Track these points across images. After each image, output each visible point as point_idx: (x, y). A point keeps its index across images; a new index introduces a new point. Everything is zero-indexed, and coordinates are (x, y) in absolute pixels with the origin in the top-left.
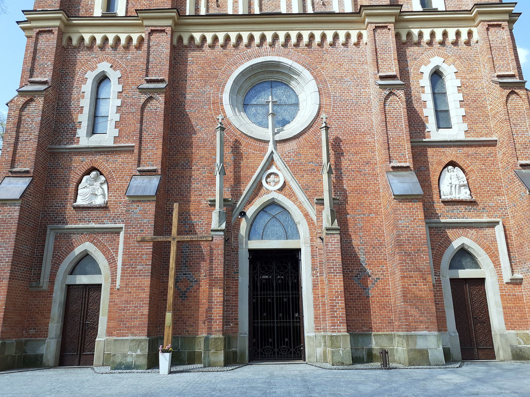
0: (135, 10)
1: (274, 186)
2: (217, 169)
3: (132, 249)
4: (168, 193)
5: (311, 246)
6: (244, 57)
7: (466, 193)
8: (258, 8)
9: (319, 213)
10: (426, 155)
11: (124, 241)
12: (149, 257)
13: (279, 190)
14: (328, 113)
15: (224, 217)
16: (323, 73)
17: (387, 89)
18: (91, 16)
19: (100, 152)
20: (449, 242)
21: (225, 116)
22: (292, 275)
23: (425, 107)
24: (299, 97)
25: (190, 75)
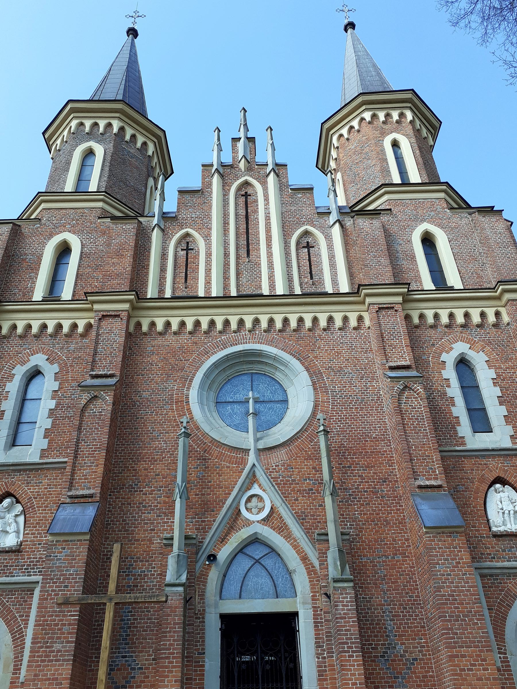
0: (84, 293)
1: (257, 514)
2: (177, 490)
3: (49, 616)
4: (107, 528)
5: (314, 607)
6: (217, 346)
9: (323, 555)
11: (39, 604)
12: (73, 629)
13: (264, 520)
14: (327, 412)
15: (184, 562)
16: (316, 363)
17: (400, 383)
18: (29, 300)
19: (19, 471)
22: (287, 655)
23: (454, 405)
24: (288, 392)
25: (149, 368)
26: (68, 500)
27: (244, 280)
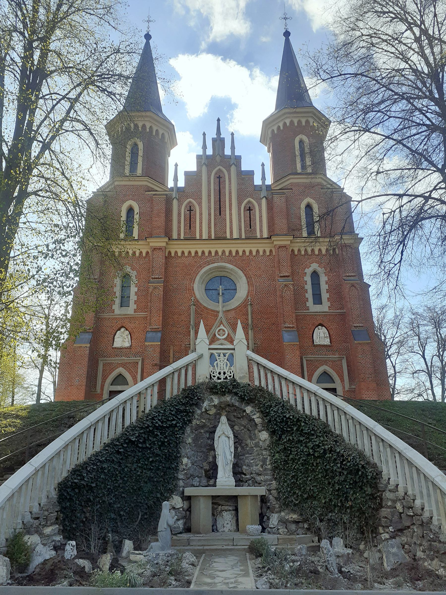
13: (225, 338)
24: (237, 285)
26: (150, 330)
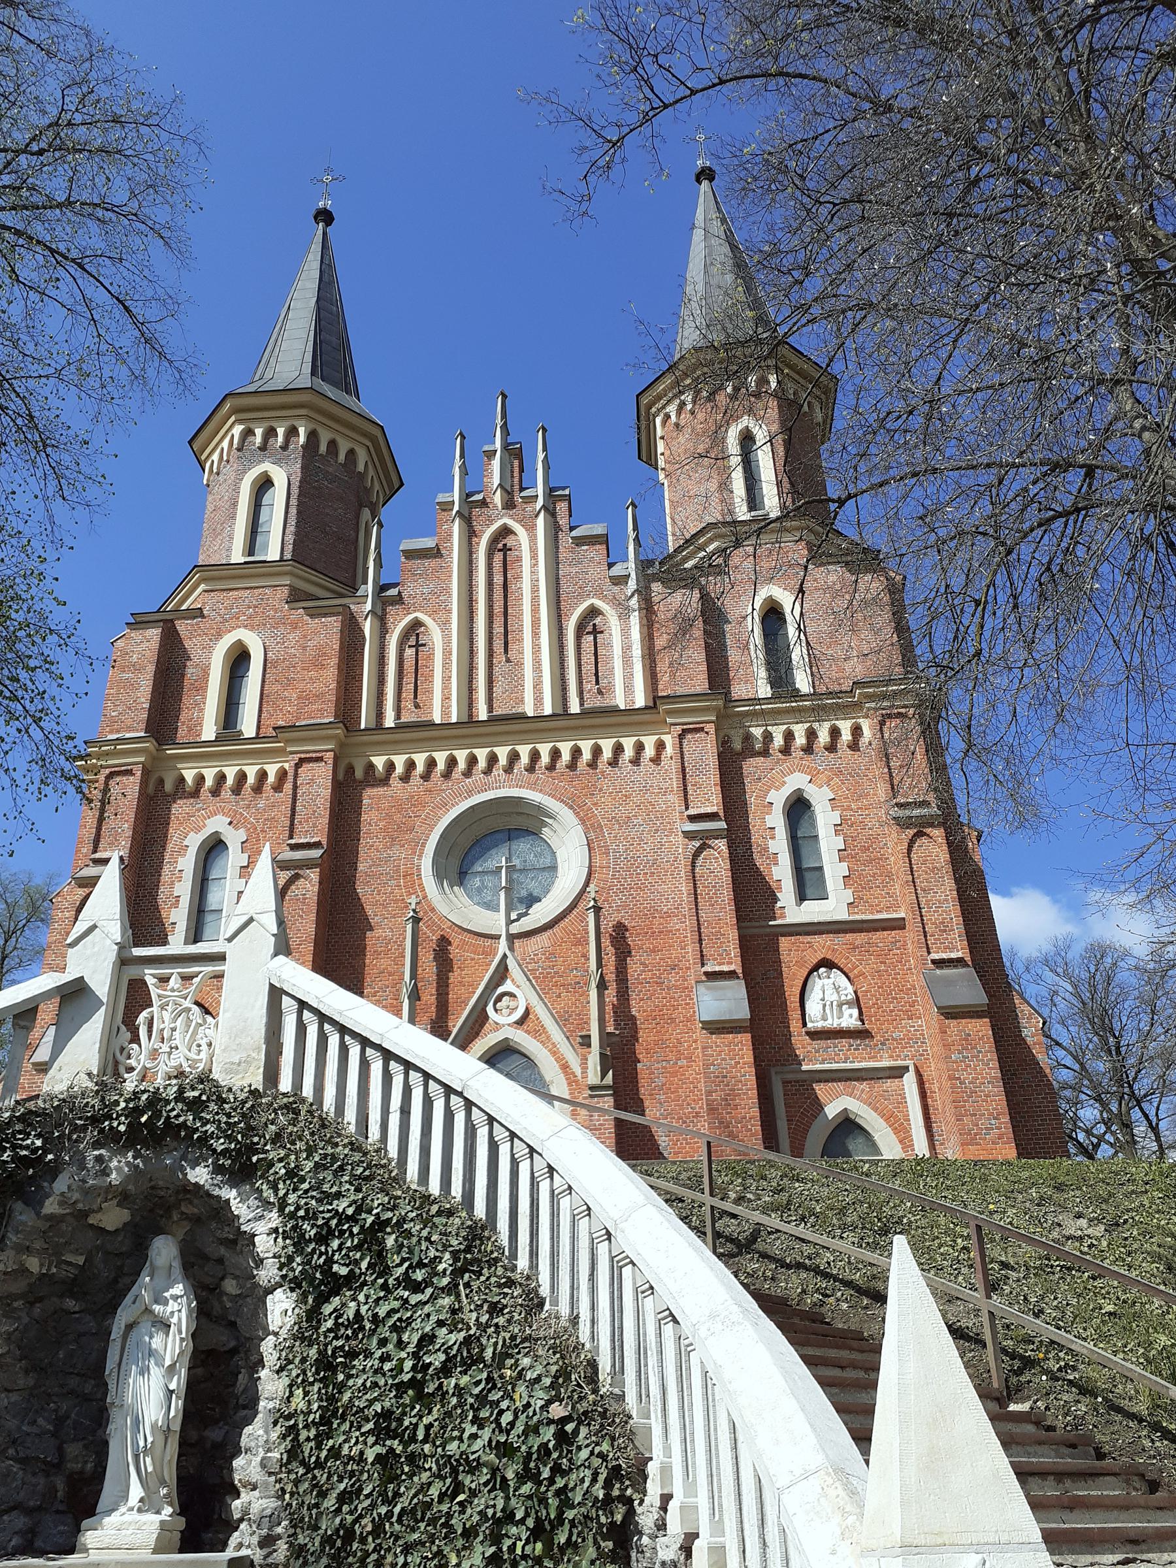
7: (851, 1016)
8: (577, 700)
10: (777, 950)
20: (818, 1107)
21: (425, 897)
24: (558, 854)
27: (500, 691)
